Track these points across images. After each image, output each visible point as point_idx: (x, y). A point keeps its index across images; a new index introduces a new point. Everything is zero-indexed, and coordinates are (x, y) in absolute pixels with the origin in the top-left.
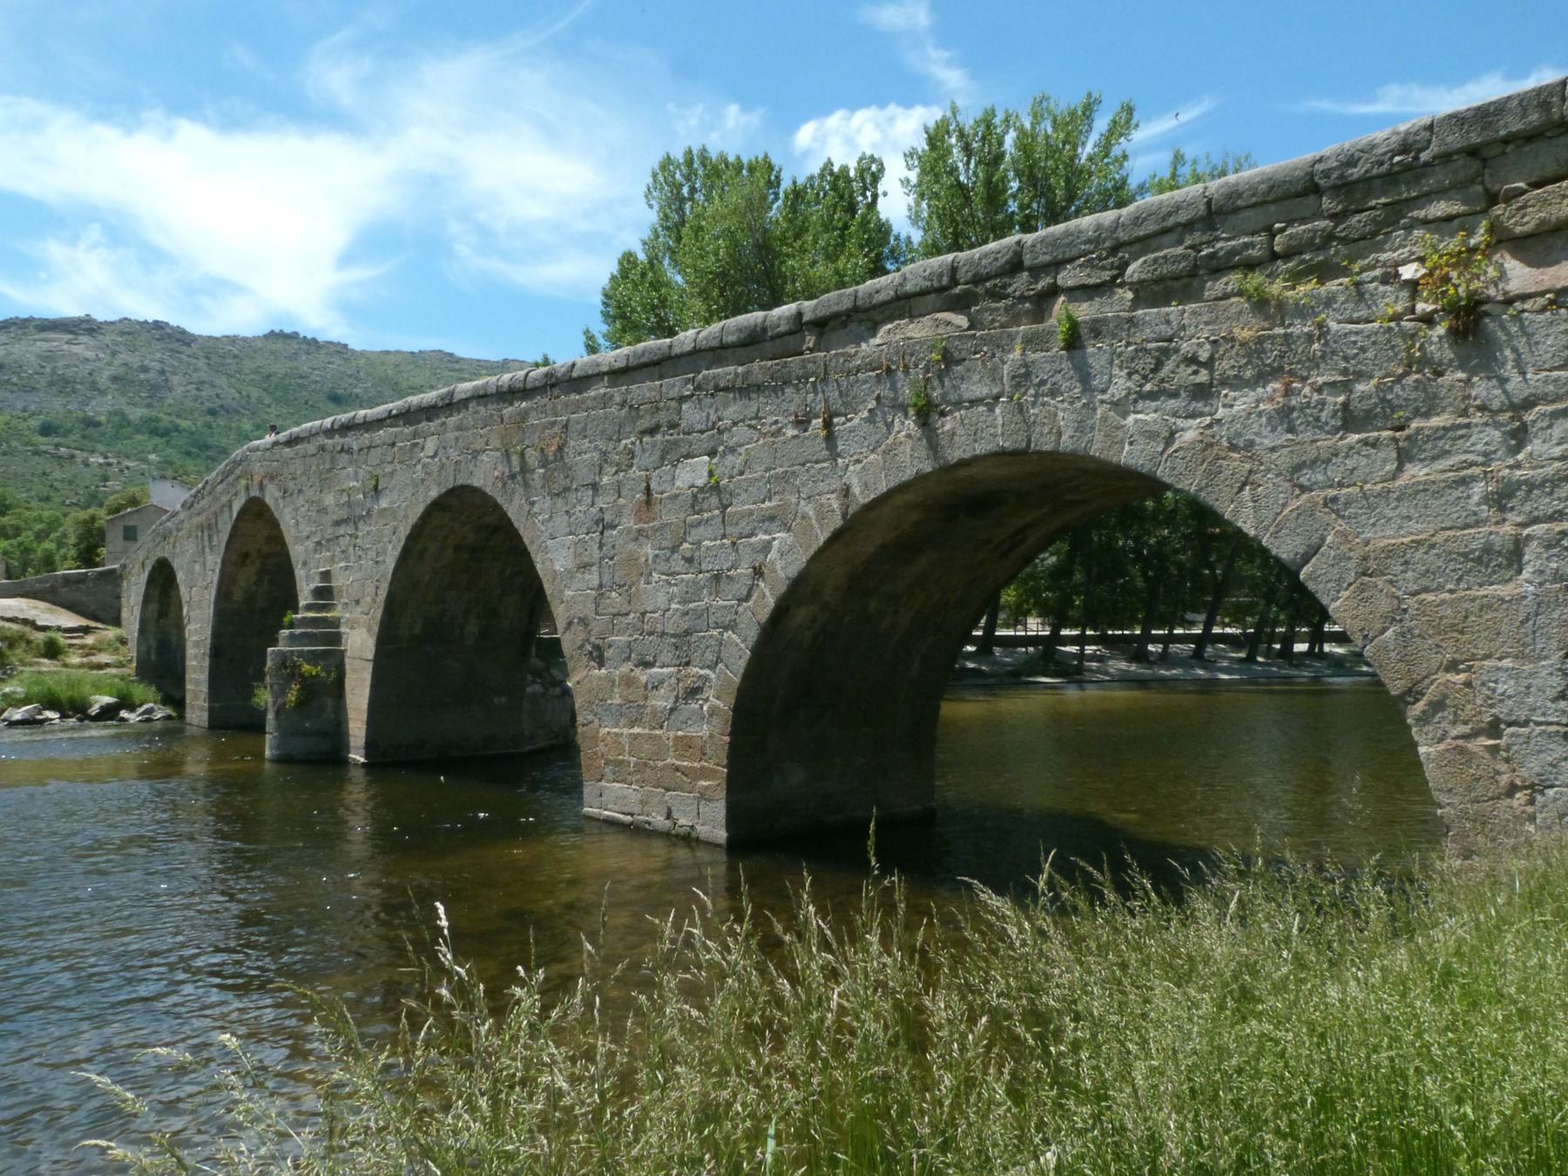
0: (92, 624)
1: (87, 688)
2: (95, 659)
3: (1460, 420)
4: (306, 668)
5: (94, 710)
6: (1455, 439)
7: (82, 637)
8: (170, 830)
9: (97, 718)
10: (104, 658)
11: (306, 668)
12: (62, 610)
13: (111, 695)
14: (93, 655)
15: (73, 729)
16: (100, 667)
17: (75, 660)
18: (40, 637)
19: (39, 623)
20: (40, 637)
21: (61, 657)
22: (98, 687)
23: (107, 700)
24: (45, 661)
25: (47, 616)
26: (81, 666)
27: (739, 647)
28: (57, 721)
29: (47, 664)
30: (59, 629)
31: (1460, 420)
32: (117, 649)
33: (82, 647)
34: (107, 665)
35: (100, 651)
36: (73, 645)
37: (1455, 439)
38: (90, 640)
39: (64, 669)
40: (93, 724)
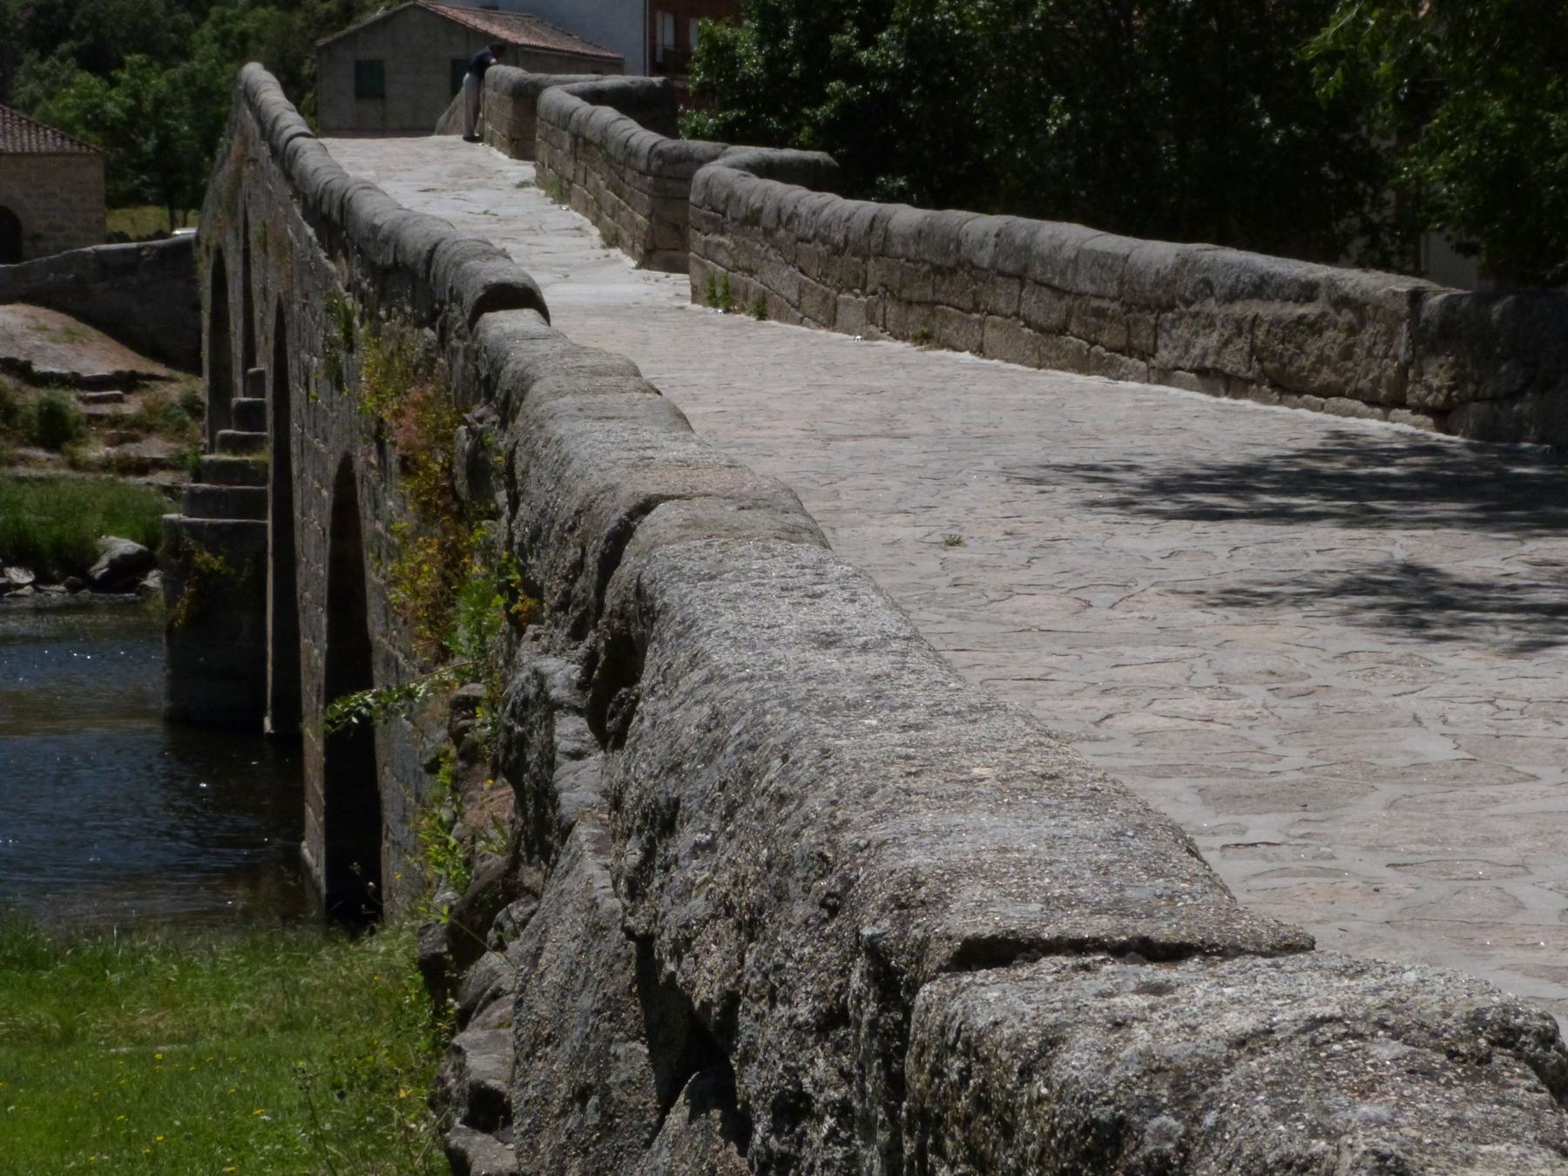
0: (145, 366)
1: (93, 522)
2: (132, 450)
3: (393, 458)
4: (203, 557)
5: (100, 569)
6: (1241, 772)
7: (119, 399)
8: (1552, 712)
9: (102, 585)
10: (154, 447)
11: (203, 557)
12: (94, 333)
13: (134, 539)
14: (135, 439)
15: (65, 609)
16: (143, 467)
17: (97, 450)
18: (31, 398)
19: (39, 367)
20: (31, 398)
21: (67, 446)
22: (115, 519)
23: (124, 546)
24: (41, 454)
25: (62, 349)
26: (106, 465)
27: (390, 816)
28: (28, 590)
29: (42, 462)
30: (74, 381)
31: (393, 458)
32: (182, 427)
33: (115, 421)
34: (158, 465)
35: (150, 430)
36: (99, 418)
37: (1241, 772)
38: (132, 406)
39: (71, 474)
40: (100, 598)
